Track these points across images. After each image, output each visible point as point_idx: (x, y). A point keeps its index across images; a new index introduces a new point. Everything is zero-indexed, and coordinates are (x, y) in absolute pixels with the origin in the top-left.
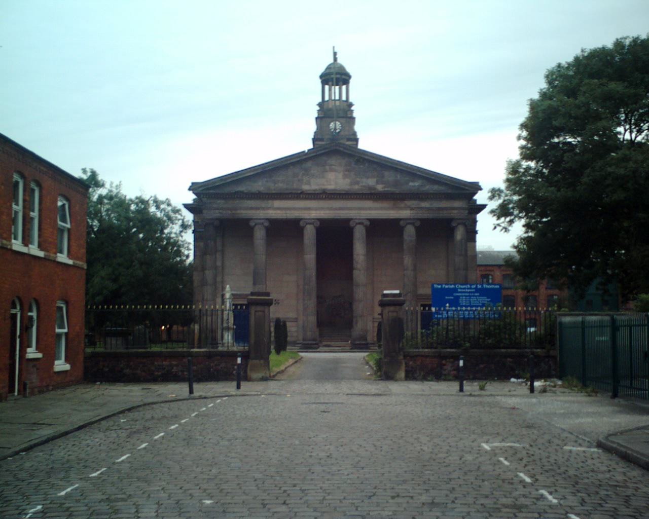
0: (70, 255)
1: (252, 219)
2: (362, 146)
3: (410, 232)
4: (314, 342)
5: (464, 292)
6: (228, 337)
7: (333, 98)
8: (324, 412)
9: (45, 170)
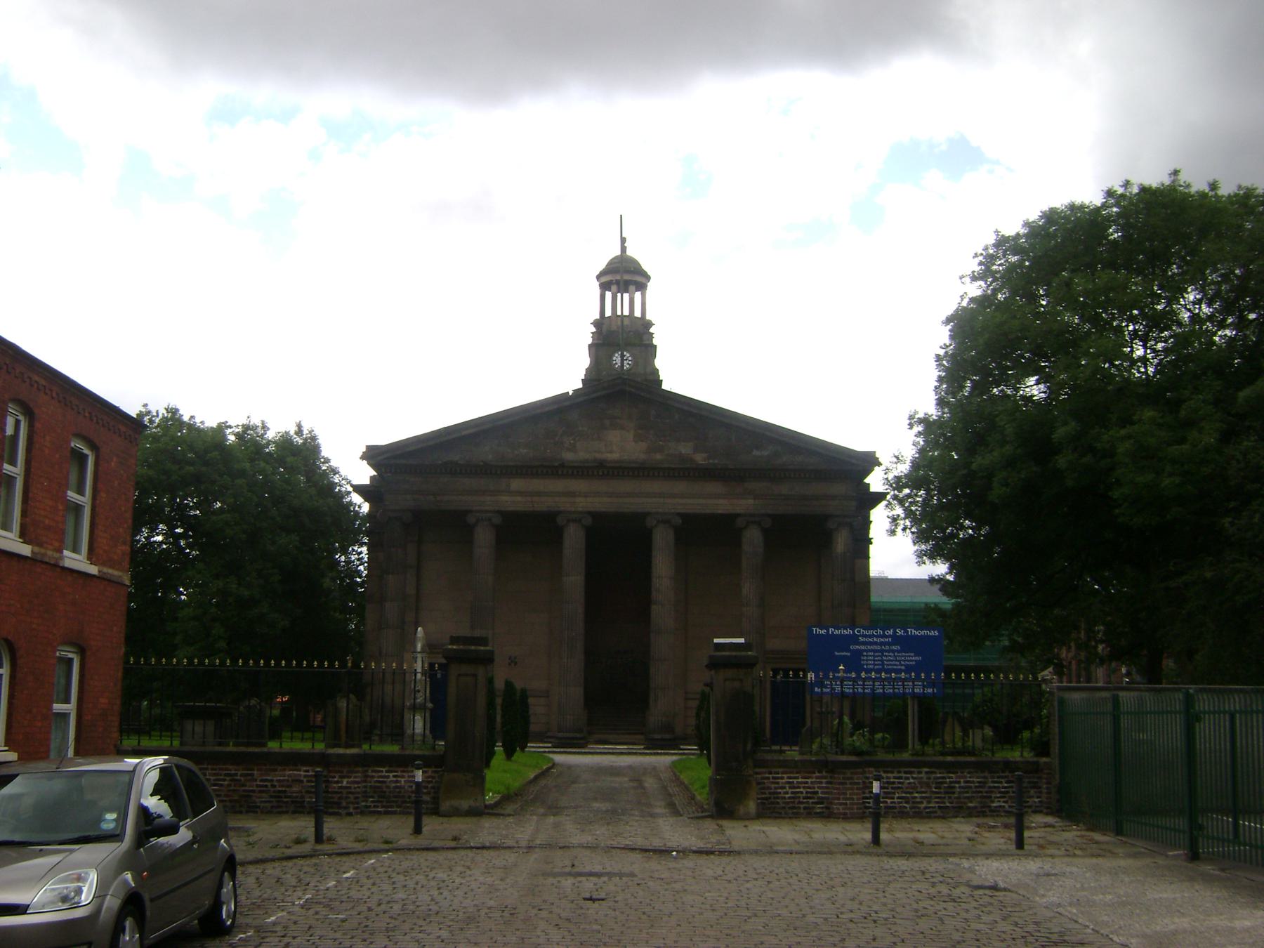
0: (92, 556)
1: (471, 511)
2: (664, 387)
3: (753, 539)
4: (578, 735)
5: (871, 644)
6: (418, 724)
7: (619, 313)
8: (590, 899)
9: (43, 382)
